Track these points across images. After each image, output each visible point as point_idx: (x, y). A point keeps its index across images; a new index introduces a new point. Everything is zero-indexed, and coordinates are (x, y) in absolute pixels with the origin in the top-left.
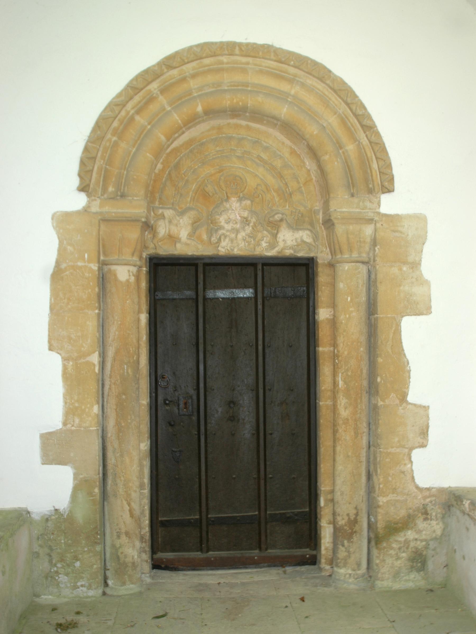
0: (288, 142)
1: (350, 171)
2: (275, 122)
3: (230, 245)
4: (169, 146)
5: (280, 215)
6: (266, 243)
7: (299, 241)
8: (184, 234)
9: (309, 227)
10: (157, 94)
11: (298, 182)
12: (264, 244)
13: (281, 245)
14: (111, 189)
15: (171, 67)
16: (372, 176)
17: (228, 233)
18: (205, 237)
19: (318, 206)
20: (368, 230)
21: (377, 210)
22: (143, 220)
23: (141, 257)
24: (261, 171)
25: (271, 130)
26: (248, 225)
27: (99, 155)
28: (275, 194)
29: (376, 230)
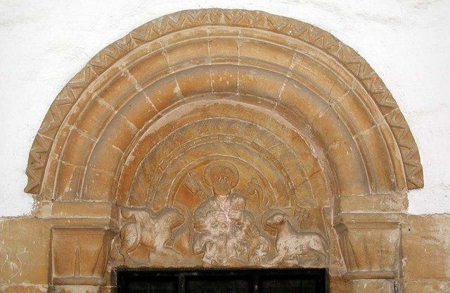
0: (289, 125)
1: (366, 162)
2: (272, 102)
3: (216, 255)
4: (141, 134)
5: (281, 217)
6: (263, 252)
7: (305, 248)
8: (159, 242)
9: (318, 231)
10: (125, 73)
11: (303, 174)
12: (260, 253)
13: (282, 253)
14: (67, 189)
15: (141, 41)
16: (394, 167)
17: (215, 240)
18: (186, 245)
19: (329, 203)
20: (393, 237)
21: (403, 212)
22: (106, 228)
23: (103, 273)
24: (256, 162)
25: (268, 111)
26: (241, 229)
27: (53, 148)
28: (274, 190)
29: (402, 236)
